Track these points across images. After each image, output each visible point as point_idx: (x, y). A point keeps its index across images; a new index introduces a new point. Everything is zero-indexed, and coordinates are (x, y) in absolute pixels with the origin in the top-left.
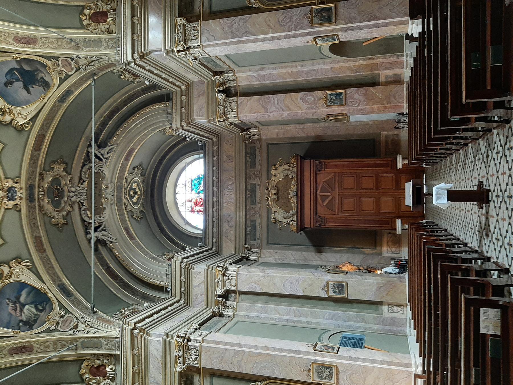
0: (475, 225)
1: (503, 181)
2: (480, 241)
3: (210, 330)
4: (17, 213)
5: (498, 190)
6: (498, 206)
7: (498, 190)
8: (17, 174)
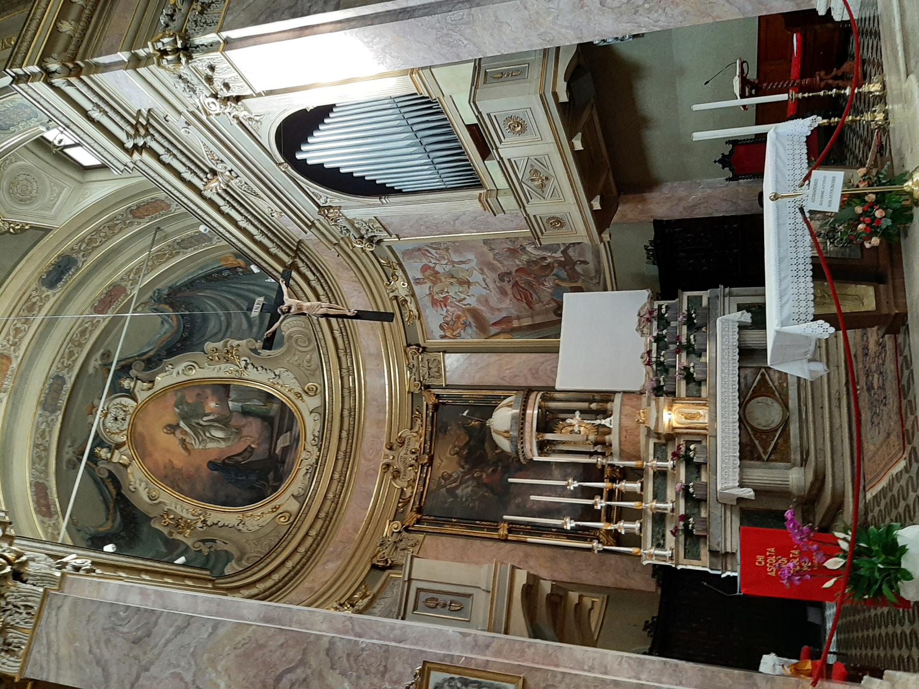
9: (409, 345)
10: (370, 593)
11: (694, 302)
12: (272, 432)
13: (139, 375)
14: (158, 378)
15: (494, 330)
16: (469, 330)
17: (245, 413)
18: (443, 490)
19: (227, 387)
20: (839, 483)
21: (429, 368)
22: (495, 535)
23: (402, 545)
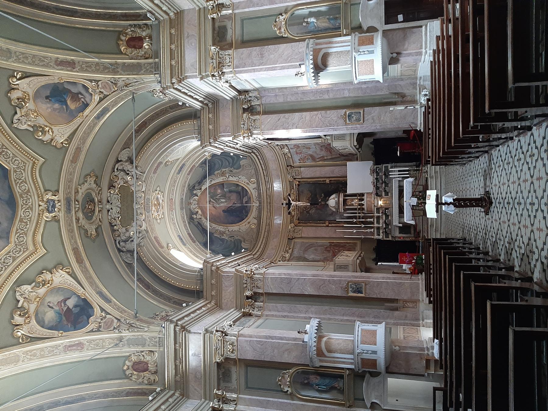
0: (489, 231)
1: (539, 186)
2: (494, 246)
3: (243, 325)
4: (57, 224)
5: (508, 197)
6: (509, 212)
7: (508, 197)
8: (56, 188)
9: (288, 166)
10: (291, 247)
11: (386, 168)
12: (241, 197)
13: (197, 188)
14: (202, 188)
15: (318, 160)
16: (309, 160)
17: (230, 192)
18: (305, 212)
19: (223, 184)
20: (420, 229)
21: (295, 173)
22: (325, 225)
23: (296, 231)
